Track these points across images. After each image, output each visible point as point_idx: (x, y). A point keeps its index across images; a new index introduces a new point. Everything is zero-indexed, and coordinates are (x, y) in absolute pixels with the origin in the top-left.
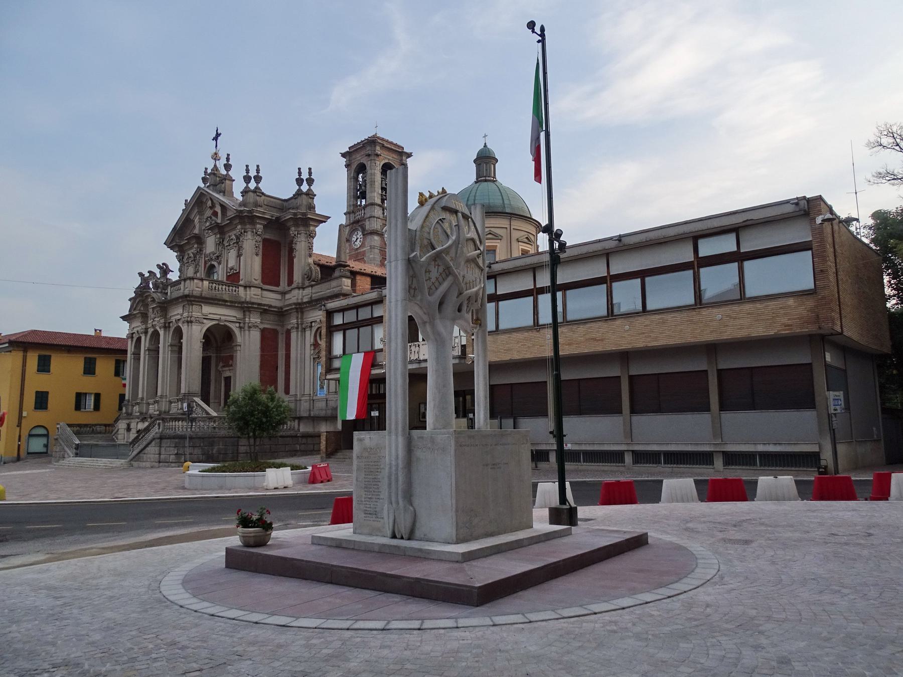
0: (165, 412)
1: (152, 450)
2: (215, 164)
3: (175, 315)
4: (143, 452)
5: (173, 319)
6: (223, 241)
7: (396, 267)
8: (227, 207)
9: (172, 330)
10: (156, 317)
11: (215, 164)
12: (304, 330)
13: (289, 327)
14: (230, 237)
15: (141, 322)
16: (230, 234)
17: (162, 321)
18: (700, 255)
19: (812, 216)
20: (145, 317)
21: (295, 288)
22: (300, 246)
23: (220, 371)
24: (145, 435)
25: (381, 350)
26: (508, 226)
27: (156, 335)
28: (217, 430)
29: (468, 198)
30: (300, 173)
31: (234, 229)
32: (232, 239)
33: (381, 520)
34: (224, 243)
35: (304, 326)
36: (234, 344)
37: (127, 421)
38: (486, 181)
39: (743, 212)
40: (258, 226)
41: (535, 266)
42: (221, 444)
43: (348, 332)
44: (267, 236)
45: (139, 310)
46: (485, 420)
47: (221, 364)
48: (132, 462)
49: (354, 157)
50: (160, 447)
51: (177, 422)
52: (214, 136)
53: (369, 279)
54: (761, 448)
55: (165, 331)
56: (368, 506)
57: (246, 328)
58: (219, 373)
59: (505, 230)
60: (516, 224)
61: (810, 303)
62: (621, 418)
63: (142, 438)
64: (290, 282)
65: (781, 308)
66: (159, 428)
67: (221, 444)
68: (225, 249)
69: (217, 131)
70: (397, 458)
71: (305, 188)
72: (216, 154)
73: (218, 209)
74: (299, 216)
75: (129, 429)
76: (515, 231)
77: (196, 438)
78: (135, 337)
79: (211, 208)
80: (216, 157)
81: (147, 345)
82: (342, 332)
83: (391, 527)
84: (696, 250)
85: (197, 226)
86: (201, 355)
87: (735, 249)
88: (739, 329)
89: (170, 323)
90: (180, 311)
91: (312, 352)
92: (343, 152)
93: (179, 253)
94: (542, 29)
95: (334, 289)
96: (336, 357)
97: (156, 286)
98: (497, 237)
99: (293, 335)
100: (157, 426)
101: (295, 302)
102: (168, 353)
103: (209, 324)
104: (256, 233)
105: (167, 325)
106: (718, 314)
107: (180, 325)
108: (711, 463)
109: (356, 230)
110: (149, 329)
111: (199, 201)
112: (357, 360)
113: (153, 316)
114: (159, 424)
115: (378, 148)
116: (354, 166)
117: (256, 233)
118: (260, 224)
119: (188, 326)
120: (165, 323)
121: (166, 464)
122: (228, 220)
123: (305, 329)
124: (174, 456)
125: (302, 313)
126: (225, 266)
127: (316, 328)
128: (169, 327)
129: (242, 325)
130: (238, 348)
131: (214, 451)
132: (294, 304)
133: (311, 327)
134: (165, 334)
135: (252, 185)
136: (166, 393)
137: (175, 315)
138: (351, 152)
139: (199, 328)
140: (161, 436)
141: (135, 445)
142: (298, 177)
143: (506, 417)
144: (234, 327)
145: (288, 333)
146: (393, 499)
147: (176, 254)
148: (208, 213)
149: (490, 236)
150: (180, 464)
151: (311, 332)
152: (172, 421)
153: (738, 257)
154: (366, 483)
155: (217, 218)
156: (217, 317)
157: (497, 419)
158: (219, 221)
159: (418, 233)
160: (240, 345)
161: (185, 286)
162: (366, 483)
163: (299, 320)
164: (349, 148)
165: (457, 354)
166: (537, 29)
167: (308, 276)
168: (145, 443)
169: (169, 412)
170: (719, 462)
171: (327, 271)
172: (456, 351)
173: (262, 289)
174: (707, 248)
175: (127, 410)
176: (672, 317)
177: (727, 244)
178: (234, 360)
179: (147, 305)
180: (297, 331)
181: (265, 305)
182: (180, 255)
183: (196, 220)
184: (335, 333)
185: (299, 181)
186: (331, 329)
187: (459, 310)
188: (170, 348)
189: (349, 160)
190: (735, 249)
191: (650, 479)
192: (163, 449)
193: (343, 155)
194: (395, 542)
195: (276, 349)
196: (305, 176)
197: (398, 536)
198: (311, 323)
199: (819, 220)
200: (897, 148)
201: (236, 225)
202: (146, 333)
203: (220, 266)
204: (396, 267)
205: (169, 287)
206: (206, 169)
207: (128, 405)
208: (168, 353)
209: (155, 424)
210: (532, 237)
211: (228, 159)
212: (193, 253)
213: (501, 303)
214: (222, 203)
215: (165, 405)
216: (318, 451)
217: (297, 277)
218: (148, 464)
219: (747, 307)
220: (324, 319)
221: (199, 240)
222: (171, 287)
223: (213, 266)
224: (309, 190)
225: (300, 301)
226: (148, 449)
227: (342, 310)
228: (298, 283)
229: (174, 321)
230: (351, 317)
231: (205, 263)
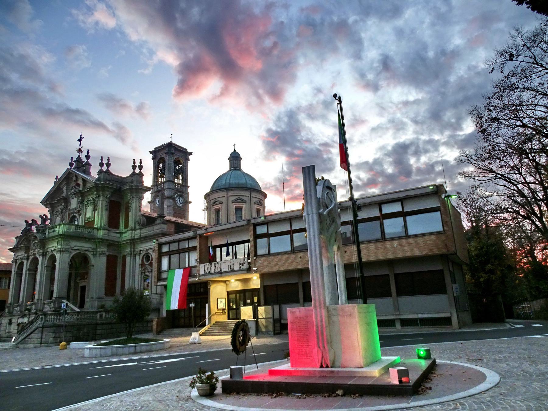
0: (40, 310)
1: (36, 336)
2: (79, 155)
3: (51, 247)
4: (29, 337)
5: (50, 250)
6: (83, 201)
7: (313, 218)
8: (87, 180)
9: (48, 257)
10: (36, 249)
11: (79, 155)
12: (135, 256)
13: (125, 254)
14: (88, 199)
15: (25, 252)
16: (88, 197)
17: (41, 251)
18: (383, 213)
19: (440, 194)
20: (27, 249)
21: (129, 230)
22: (134, 205)
23: (78, 283)
24: (30, 326)
25: (195, 267)
26: (249, 196)
27: (35, 260)
28: (83, 320)
29: (226, 179)
30: (134, 162)
31: (92, 194)
32: (90, 200)
33: (311, 358)
34: (84, 202)
35: (135, 253)
36: (90, 265)
37: (10, 318)
38: (236, 170)
39: (405, 191)
40: (107, 193)
41: (291, 218)
42: (85, 329)
43: (172, 256)
44: (112, 199)
45: (24, 244)
46: (346, 300)
47: (79, 278)
48: (18, 345)
49: (157, 154)
50: (42, 333)
51: (51, 317)
52: (82, 140)
53: (173, 225)
54: (420, 316)
55: (43, 257)
56: (301, 350)
57: (98, 255)
58: (76, 284)
59: (247, 197)
60: (254, 194)
61: (442, 238)
62: (392, 299)
63: (27, 328)
64: (126, 226)
65: (427, 241)
66: (41, 321)
67: (85, 329)
68: (84, 206)
69: (81, 136)
70: (322, 321)
71: (137, 171)
72: (80, 149)
73: (80, 182)
74: (133, 188)
75: (10, 323)
76: (253, 198)
77: (69, 326)
78: (19, 262)
79: (75, 181)
80: (79, 151)
81: (28, 267)
82: (168, 256)
83: (320, 361)
84: (381, 210)
85: (65, 192)
86: (68, 272)
87: (401, 210)
88: (406, 252)
89: (46, 252)
90: (56, 244)
91: (140, 269)
92: (151, 150)
93: (50, 209)
94: (340, 98)
95: (156, 231)
96: (164, 271)
97: (38, 230)
98: (243, 201)
99: (128, 259)
100: (40, 319)
101: (130, 238)
102: (44, 271)
103: (74, 253)
104: (106, 197)
105: (45, 253)
106: (395, 244)
107: (55, 253)
108: (394, 325)
109: (158, 196)
110: (30, 257)
111: (68, 177)
112: (179, 274)
113: (34, 248)
114: (42, 318)
115: (173, 149)
116: (157, 159)
117: (106, 197)
118: (108, 191)
119: (61, 254)
120: (43, 253)
121: (46, 344)
122: (88, 189)
123: (136, 255)
124: (52, 339)
125: (134, 245)
126: (84, 217)
127: (143, 255)
128: (46, 255)
129: (95, 253)
130: (92, 268)
131: (81, 334)
132: (130, 240)
133: (140, 253)
134: (42, 260)
135: (105, 168)
136: (42, 297)
137: (51, 247)
138: (156, 151)
139: (68, 255)
140: (43, 326)
141: (21, 333)
142: (133, 164)
143: (275, 304)
144: (90, 255)
145: (124, 257)
146: (321, 345)
147: (48, 209)
148: (73, 184)
149: (239, 201)
150: (57, 344)
151: (140, 257)
152: (50, 316)
153: (403, 214)
154: (298, 337)
155: (80, 187)
156: (79, 248)
157: (271, 305)
158: (81, 189)
159: (321, 200)
160: (93, 266)
161: (59, 228)
162: (298, 337)
163: (132, 250)
164: (155, 149)
165: (245, 268)
166: (337, 98)
167: (137, 223)
168: (30, 331)
169: (42, 310)
170: (398, 325)
171: (149, 221)
172: (245, 266)
173: (109, 231)
174: (387, 209)
175: (9, 310)
176: (370, 246)
177: (396, 208)
178: (89, 275)
179: (30, 241)
180: (131, 257)
181: (110, 240)
182: (51, 210)
183: (65, 188)
184: (163, 257)
185: (134, 167)
186: (161, 255)
187: (335, 241)
188: (46, 268)
189: (155, 155)
190: (401, 210)
191: (171, 354)
192: (44, 335)
193: (151, 152)
194: (321, 369)
195: (116, 267)
196: (137, 164)
197: (324, 366)
198: (140, 251)
199: (443, 196)
200: (469, 162)
201: (94, 192)
202: (28, 259)
203: (81, 217)
204: (313, 218)
205: (48, 230)
206: (72, 158)
207: (10, 307)
208: (44, 271)
209: (39, 318)
210: (262, 201)
211: (88, 152)
212: (60, 208)
213: (271, 238)
214: (84, 178)
215: (41, 306)
216: (151, 331)
217: (131, 224)
218: (32, 346)
219: (410, 240)
220: (157, 249)
221: (67, 201)
222: (49, 230)
223: (74, 217)
224: (140, 172)
225: (133, 238)
226: (32, 335)
227: (169, 243)
228: (132, 227)
229: (50, 251)
230: (174, 247)
231: (69, 214)
